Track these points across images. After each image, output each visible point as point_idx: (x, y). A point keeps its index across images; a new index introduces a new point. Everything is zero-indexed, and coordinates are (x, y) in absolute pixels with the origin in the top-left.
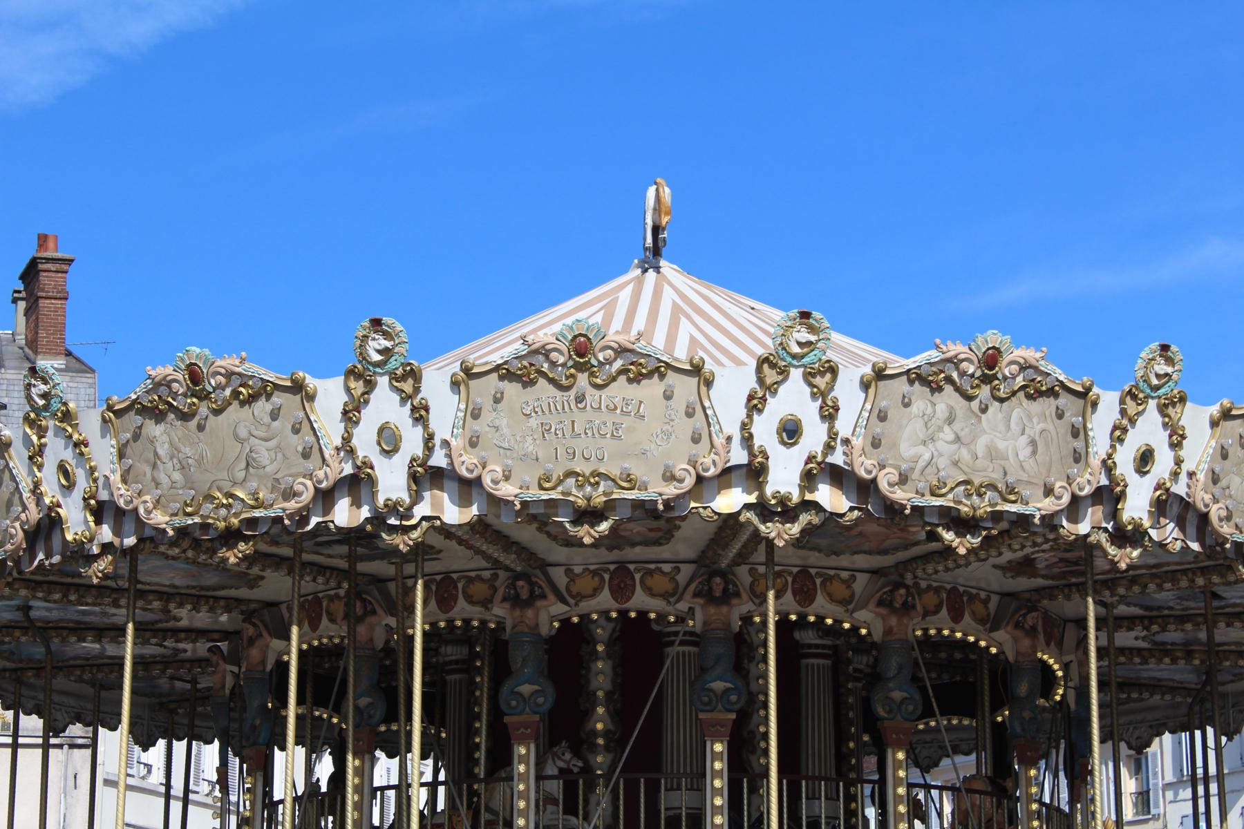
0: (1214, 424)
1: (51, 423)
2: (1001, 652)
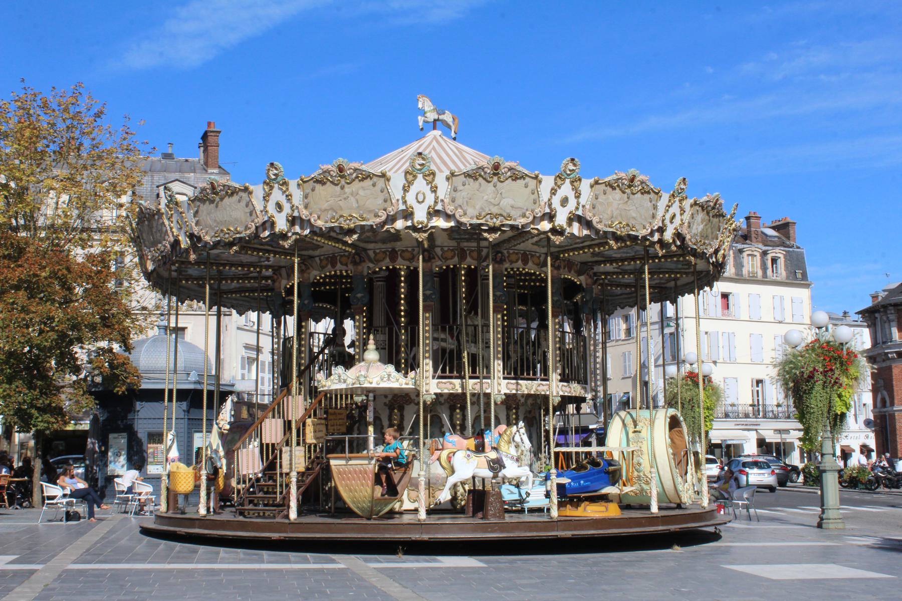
0: (592, 186)
1: (276, 186)
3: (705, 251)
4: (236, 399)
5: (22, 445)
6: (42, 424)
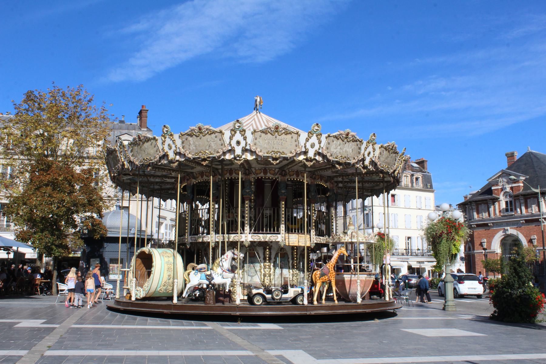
1: (167, 136)
2: (327, 187)
3: (388, 171)
4: (153, 243)
5: (47, 263)
6: (58, 253)
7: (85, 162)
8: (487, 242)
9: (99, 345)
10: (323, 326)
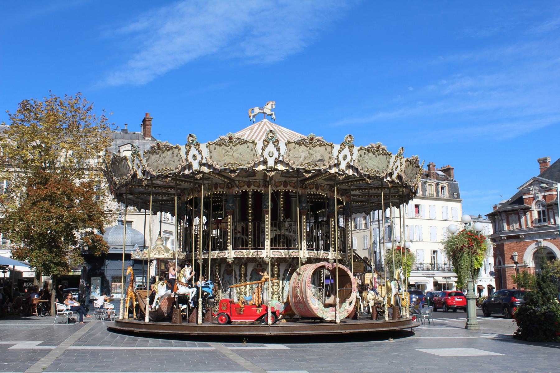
0: (359, 151)
7: (85, 174)
8: (519, 256)
9: (96, 367)
10: (333, 346)
